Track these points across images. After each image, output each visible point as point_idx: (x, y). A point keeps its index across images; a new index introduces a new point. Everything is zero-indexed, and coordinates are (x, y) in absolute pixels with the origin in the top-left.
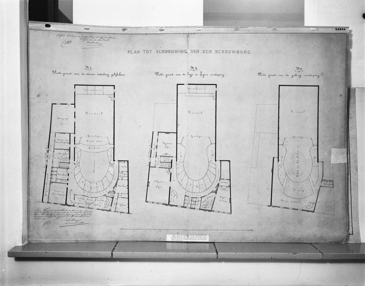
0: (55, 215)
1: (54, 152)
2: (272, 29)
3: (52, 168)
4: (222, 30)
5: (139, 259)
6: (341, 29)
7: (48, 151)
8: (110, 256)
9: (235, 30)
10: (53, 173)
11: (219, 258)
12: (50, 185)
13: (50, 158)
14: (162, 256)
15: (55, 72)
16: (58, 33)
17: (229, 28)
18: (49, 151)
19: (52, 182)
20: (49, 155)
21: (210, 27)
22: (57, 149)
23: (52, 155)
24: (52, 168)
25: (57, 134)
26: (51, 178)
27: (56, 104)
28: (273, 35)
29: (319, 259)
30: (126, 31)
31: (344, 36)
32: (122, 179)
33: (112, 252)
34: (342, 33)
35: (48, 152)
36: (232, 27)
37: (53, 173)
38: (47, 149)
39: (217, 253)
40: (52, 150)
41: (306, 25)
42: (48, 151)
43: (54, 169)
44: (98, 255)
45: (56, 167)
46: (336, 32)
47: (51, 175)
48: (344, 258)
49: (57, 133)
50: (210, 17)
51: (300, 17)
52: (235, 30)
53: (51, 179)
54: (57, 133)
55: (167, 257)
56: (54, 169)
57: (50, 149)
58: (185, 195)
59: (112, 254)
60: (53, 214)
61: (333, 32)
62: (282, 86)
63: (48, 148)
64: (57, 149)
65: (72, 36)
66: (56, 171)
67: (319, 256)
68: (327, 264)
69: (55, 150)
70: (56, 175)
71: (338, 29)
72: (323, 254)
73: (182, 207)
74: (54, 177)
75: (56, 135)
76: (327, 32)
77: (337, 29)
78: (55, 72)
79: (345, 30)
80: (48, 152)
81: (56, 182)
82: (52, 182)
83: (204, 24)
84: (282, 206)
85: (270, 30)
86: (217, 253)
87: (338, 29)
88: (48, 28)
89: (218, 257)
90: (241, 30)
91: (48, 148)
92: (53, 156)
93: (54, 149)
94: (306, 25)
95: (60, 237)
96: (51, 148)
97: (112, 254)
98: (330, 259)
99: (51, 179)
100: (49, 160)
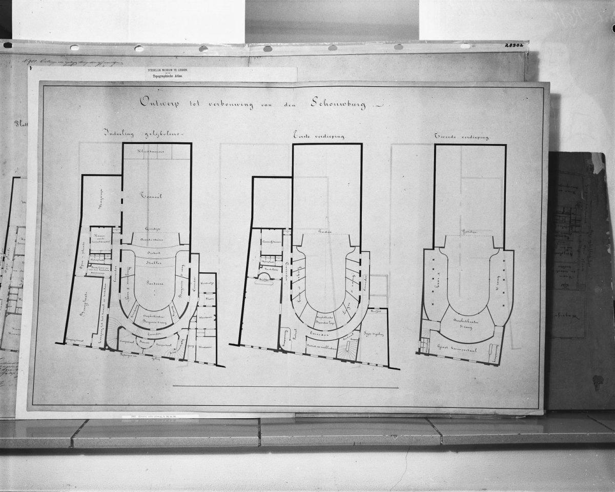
0: (12, 372)
1: (13, 260)
2: (393, 45)
3: (10, 287)
4: (307, 49)
5: (162, 449)
6: (514, 45)
7: (4, 258)
8: (67, 445)
9: (330, 49)
10: (12, 297)
11: (262, 445)
12: (5, 319)
13: (8, 271)
14: (162, 444)
15: (19, 123)
16: (25, 57)
17: (320, 45)
18: (5, 258)
19: (9, 313)
20: (5, 265)
21: (303, 45)
22: (18, 255)
23: (10, 264)
24: (10, 287)
25: (19, 229)
26: (7, 305)
27: (20, 177)
28: (395, 56)
29: (436, 445)
30: (205, 51)
31: (520, 56)
32: (368, 308)
33: (73, 437)
34: (517, 52)
35: (3, 260)
36: (324, 45)
37: (12, 297)
38: (3, 255)
39: (260, 437)
40: (11, 257)
41: (421, 38)
42: (4, 258)
43: (14, 291)
44: (45, 444)
45: (16, 287)
46: (506, 51)
47: (8, 300)
48: (476, 442)
49: (21, 227)
50: (256, 28)
51: (410, 31)
52: (330, 49)
53: (7, 307)
54: (21, 227)
55: (171, 445)
56: (14, 291)
57: (7, 255)
58: (306, 336)
59: (72, 441)
60: (8, 368)
61: (501, 51)
62: (124, 156)
63: (4, 253)
64: (18, 255)
65: (49, 61)
66: (17, 293)
67: (435, 439)
68: (448, 453)
69: (16, 257)
70: (17, 301)
71: (511, 45)
72: (441, 435)
73: (334, 359)
74: (13, 303)
75: (19, 230)
76: (490, 51)
77: (509, 45)
78: (19, 123)
79: (522, 46)
80: (3, 260)
81: (15, 314)
82: (9, 313)
83: (247, 41)
84: (265, 347)
85: (391, 48)
86: (260, 437)
87: (511, 45)
88: (9, 50)
89: (260, 444)
90: (342, 49)
91: (4, 253)
92: (12, 268)
93: (14, 255)
94: (421, 38)
95: (474, 430)
96: (10, 254)
97: (72, 441)
98: (454, 444)
99: (7, 307)
100: (4, 275)
